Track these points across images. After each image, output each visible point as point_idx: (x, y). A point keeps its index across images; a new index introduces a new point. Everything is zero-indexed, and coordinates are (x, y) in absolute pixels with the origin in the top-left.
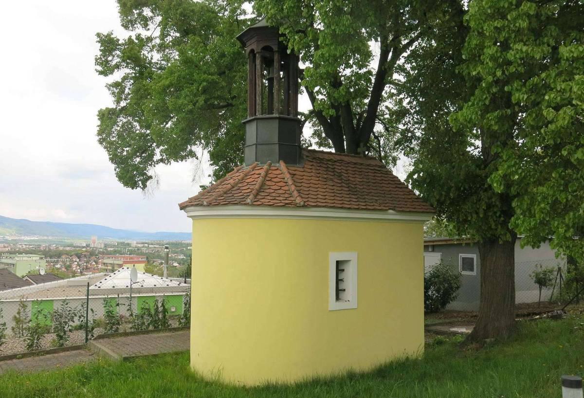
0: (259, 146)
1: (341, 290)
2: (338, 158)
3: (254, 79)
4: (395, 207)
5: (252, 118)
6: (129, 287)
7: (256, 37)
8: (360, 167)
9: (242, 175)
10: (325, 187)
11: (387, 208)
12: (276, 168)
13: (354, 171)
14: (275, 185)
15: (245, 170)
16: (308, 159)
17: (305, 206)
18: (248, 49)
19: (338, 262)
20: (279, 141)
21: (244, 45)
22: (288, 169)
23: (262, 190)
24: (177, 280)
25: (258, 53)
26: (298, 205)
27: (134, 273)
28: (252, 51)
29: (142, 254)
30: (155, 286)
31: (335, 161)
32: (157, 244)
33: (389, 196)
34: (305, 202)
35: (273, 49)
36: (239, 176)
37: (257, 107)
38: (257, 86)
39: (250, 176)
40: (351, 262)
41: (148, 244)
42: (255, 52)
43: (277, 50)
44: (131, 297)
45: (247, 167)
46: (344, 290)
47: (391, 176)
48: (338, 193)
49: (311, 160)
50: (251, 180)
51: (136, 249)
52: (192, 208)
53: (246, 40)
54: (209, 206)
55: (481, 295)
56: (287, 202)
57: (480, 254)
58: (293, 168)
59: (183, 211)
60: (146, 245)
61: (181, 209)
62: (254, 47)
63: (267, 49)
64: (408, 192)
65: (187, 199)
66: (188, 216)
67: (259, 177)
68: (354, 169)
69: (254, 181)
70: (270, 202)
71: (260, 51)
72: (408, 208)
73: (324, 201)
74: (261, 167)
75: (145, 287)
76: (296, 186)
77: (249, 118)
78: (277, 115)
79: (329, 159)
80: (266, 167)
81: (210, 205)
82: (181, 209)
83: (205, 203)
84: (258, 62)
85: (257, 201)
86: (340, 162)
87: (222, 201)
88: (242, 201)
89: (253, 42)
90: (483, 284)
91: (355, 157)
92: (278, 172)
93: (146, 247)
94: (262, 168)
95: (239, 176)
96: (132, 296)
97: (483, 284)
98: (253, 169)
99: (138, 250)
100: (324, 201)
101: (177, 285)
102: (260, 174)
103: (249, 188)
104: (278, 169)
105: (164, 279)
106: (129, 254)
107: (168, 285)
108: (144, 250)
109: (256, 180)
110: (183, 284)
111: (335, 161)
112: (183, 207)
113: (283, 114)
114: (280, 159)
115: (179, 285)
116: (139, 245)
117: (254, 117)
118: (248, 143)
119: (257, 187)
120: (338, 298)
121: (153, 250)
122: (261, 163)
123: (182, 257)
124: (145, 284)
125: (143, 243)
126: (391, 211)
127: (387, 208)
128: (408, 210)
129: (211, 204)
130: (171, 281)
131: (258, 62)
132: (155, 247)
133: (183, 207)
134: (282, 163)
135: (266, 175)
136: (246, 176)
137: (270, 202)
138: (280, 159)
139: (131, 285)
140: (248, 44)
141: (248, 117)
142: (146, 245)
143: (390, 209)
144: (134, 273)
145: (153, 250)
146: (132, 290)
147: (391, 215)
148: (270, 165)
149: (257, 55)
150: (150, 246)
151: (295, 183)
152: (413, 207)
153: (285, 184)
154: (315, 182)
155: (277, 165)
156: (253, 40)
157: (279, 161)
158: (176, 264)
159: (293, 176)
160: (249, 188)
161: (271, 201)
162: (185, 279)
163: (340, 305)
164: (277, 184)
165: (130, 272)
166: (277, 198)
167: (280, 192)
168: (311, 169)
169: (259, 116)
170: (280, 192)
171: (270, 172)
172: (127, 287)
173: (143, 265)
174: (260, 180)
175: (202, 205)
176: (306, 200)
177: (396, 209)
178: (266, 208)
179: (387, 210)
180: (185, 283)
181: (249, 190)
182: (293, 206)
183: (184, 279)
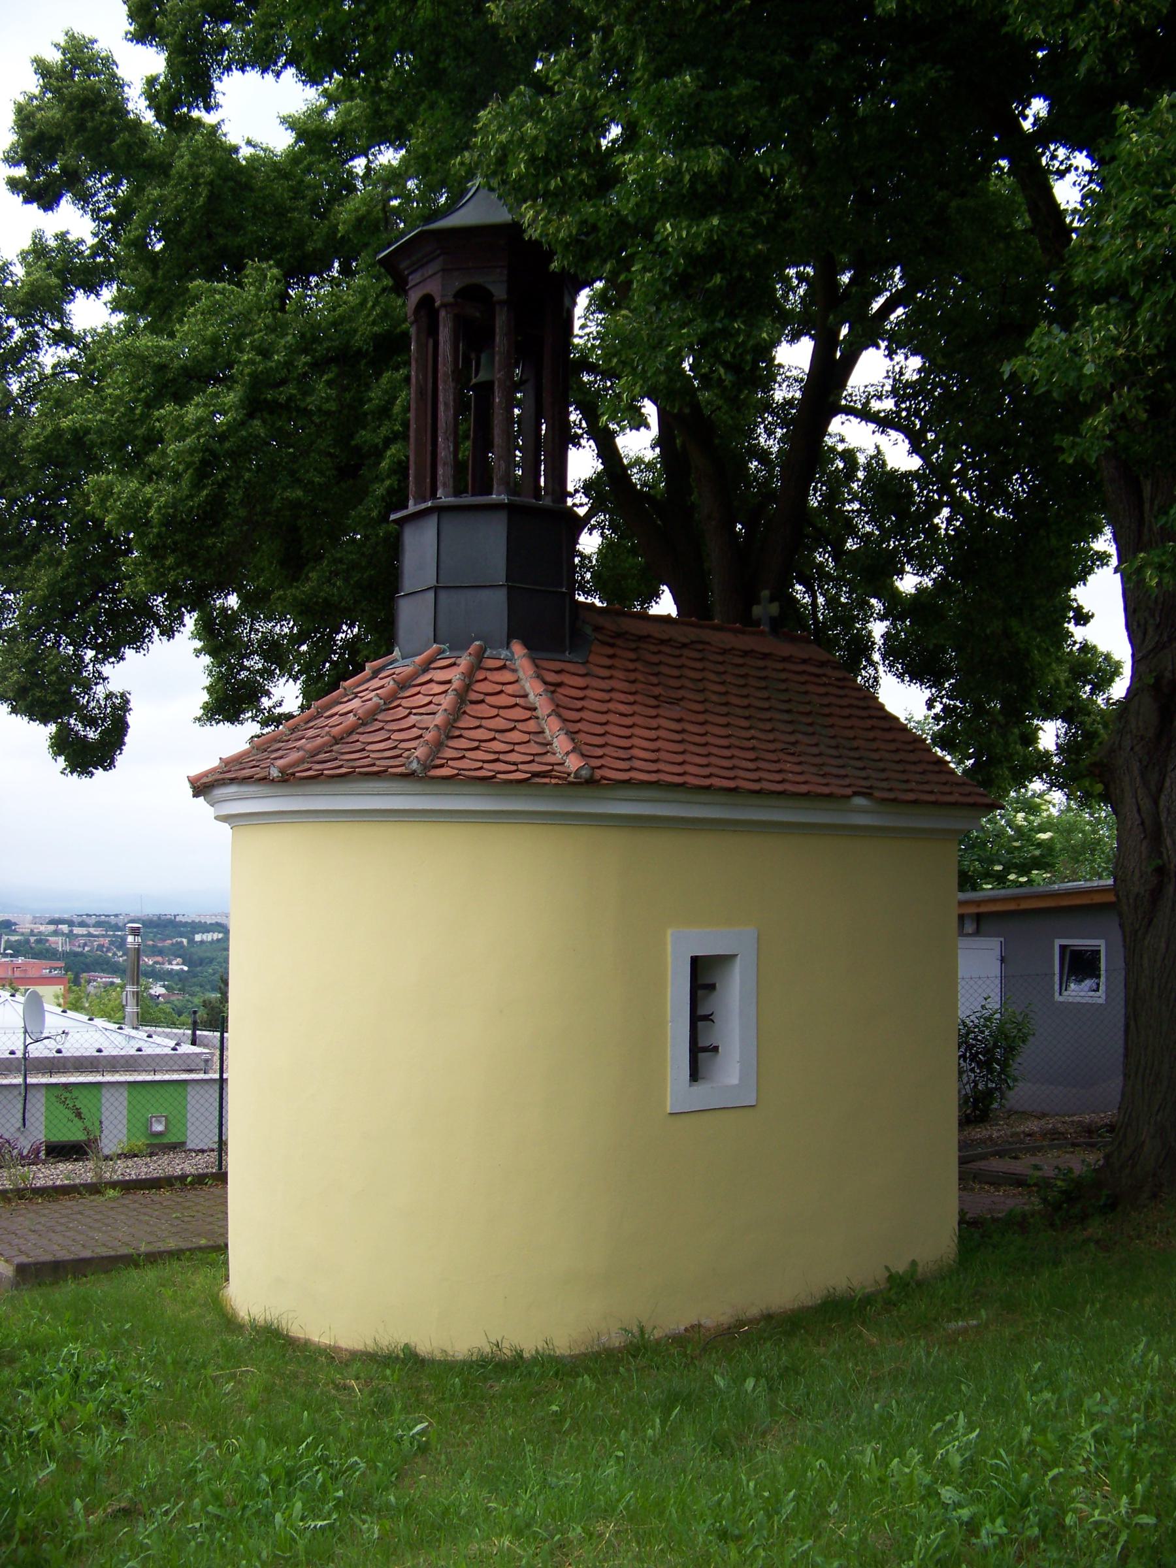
0: (443, 595)
1: (705, 1050)
2: (692, 633)
3: (430, 385)
4: (871, 787)
5: (423, 506)
6: (19, 1054)
7: (441, 258)
8: (761, 663)
9: (390, 684)
10: (654, 723)
11: (849, 791)
12: (499, 663)
13: (742, 676)
14: (497, 715)
15: (398, 671)
16: (600, 637)
17: (590, 783)
18: (414, 297)
19: (695, 961)
20: (508, 578)
21: (400, 288)
22: (537, 666)
23: (457, 733)
24: (167, 1036)
25: (444, 305)
26: (571, 779)
27: (35, 1008)
28: (426, 302)
29: (47, 954)
30: (99, 1051)
31: (684, 645)
32: (98, 924)
33: (852, 754)
34: (593, 768)
35: (491, 295)
36: (382, 687)
37: (440, 471)
38: (441, 408)
39: (417, 689)
40: (738, 959)
41: (70, 923)
42: (437, 304)
43: (504, 296)
44: (26, 1085)
45: (407, 661)
46: (715, 1049)
47: (880, 714)
48: (695, 744)
49: (611, 641)
50: (422, 700)
51: (32, 939)
52: (232, 789)
53: (407, 268)
54: (285, 781)
55: (1126, 1056)
56: (535, 768)
57: (1124, 932)
58: (558, 666)
59: (202, 798)
60: (64, 928)
61: (196, 794)
62: (434, 287)
63: (472, 294)
64: (909, 743)
65: (216, 763)
66: (217, 818)
67: (446, 692)
68: (742, 671)
69: (430, 703)
70: (481, 768)
71: (451, 300)
72: (911, 790)
73: (654, 767)
74: (452, 660)
75: (65, 1053)
76: (565, 720)
77: (412, 508)
78: (504, 498)
79: (665, 637)
80: (464, 661)
81: (288, 779)
82: (196, 794)
83: (275, 773)
84: (445, 333)
85: (442, 766)
86: (700, 647)
87: (329, 765)
88: (392, 767)
89: (430, 273)
90: (1132, 1023)
91: (743, 633)
92: (507, 676)
93: (63, 934)
94: (454, 664)
95: (382, 687)
96: (30, 1080)
97: (1132, 1023)
98: (426, 667)
99: (38, 941)
100: (654, 767)
101: (168, 1051)
102: (449, 682)
103: (414, 726)
104: (504, 667)
105: (128, 1030)
106: (12, 956)
107: (139, 1050)
108: (58, 943)
109: (436, 700)
110: (187, 1048)
111: (684, 645)
112: (202, 787)
113: (519, 495)
114: (510, 636)
115: (174, 1049)
116: (42, 928)
117: (429, 504)
118: (409, 583)
119: (439, 719)
120: (695, 1075)
121: (85, 945)
122: (451, 649)
123: (177, 966)
124: (67, 1045)
125: (54, 922)
126: (859, 801)
127: (849, 791)
128: (911, 796)
129: (293, 774)
130: (150, 1036)
131: (445, 333)
132: (90, 935)
133: (202, 787)
134: (518, 649)
135: (468, 688)
136: (364, 724)
137: (481, 768)
138: (510, 636)
139: (26, 1047)
140: (413, 279)
141: (411, 502)
142: (64, 928)
143: (855, 794)
144: (35, 1008)
145: (85, 945)
146: (27, 1065)
147: (861, 811)
148: (480, 656)
149: (443, 313)
150: (77, 930)
151: (562, 711)
152: (927, 788)
153: (528, 714)
154: (623, 708)
155: (504, 653)
156: (430, 270)
157: (508, 644)
158: (158, 990)
159: (552, 688)
160: (414, 726)
161: (486, 766)
162: (194, 1034)
163: (702, 1094)
164: (502, 712)
165: (20, 1008)
166: (502, 757)
167: (515, 736)
168: (609, 667)
169: (444, 497)
170: (515, 736)
171: (480, 675)
172: (12, 1053)
173: (59, 989)
174: (447, 701)
175: (265, 780)
176: (597, 763)
177: (877, 794)
178: (466, 789)
179: (848, 797)
180: (194, 1043)
181: (415, 732)
182: (554, 781)
183: (190, 1032)
